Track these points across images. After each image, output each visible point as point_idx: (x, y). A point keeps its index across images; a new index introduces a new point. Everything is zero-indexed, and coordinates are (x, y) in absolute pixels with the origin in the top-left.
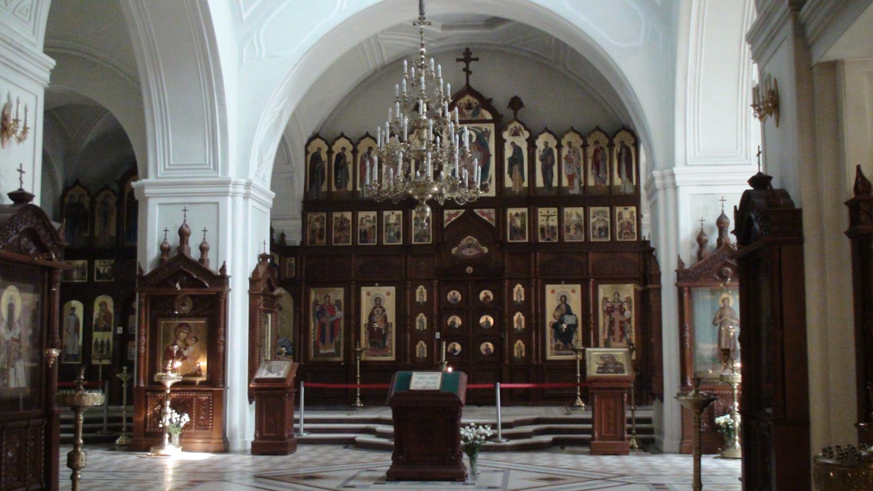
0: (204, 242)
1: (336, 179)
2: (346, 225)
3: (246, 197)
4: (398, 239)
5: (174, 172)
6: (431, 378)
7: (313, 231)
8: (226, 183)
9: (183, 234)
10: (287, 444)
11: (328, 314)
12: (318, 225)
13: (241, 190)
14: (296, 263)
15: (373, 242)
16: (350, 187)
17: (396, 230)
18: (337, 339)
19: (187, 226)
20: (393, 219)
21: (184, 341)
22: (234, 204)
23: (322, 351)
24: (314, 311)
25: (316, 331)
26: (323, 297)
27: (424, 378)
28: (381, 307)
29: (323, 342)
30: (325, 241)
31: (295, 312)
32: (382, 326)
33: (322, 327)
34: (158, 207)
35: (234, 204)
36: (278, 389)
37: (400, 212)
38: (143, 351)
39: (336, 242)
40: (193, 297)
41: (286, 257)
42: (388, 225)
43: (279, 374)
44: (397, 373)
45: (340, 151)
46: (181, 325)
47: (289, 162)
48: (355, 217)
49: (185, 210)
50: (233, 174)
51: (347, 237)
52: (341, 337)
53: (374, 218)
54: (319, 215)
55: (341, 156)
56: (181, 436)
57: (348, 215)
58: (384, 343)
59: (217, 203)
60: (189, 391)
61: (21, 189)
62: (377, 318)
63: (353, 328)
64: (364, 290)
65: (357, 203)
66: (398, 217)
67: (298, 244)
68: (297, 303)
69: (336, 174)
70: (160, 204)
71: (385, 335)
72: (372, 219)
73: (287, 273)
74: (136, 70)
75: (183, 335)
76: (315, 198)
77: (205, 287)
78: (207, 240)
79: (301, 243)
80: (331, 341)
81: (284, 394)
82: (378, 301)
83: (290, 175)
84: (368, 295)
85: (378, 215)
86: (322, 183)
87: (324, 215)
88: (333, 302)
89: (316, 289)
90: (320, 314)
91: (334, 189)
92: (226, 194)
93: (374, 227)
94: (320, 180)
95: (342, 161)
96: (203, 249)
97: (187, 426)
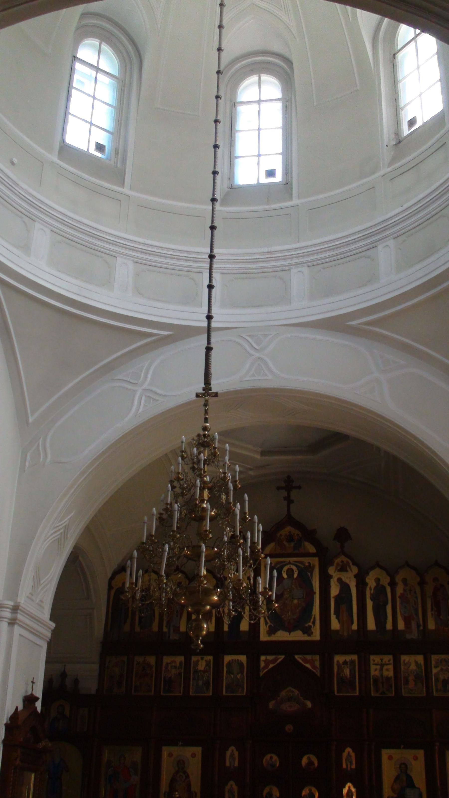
3: (12, 623)
16: (155, 627)
20: (202, 666)
28: (185, 772)
37: (211, 658)
42: (196, 671)
48: (159, 662)
53: (181, 663)
57: (152, 660)
61: (32, 694)
64: (166, 750)
66: (208, 663)
67: (93, 692)
72: (178, 665)
82: (181, 765)
84: (169, 755)
91: (137, 629)
93: (180, 674)
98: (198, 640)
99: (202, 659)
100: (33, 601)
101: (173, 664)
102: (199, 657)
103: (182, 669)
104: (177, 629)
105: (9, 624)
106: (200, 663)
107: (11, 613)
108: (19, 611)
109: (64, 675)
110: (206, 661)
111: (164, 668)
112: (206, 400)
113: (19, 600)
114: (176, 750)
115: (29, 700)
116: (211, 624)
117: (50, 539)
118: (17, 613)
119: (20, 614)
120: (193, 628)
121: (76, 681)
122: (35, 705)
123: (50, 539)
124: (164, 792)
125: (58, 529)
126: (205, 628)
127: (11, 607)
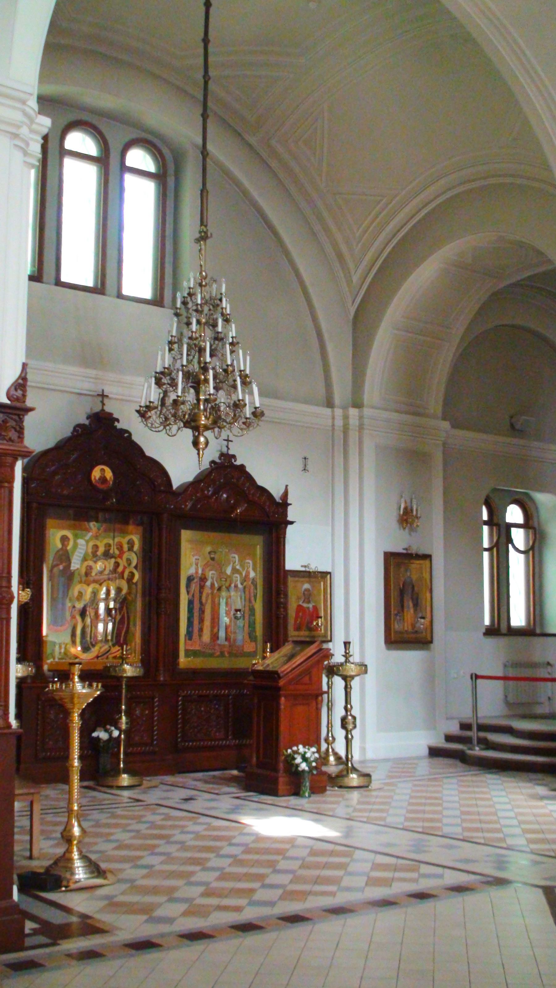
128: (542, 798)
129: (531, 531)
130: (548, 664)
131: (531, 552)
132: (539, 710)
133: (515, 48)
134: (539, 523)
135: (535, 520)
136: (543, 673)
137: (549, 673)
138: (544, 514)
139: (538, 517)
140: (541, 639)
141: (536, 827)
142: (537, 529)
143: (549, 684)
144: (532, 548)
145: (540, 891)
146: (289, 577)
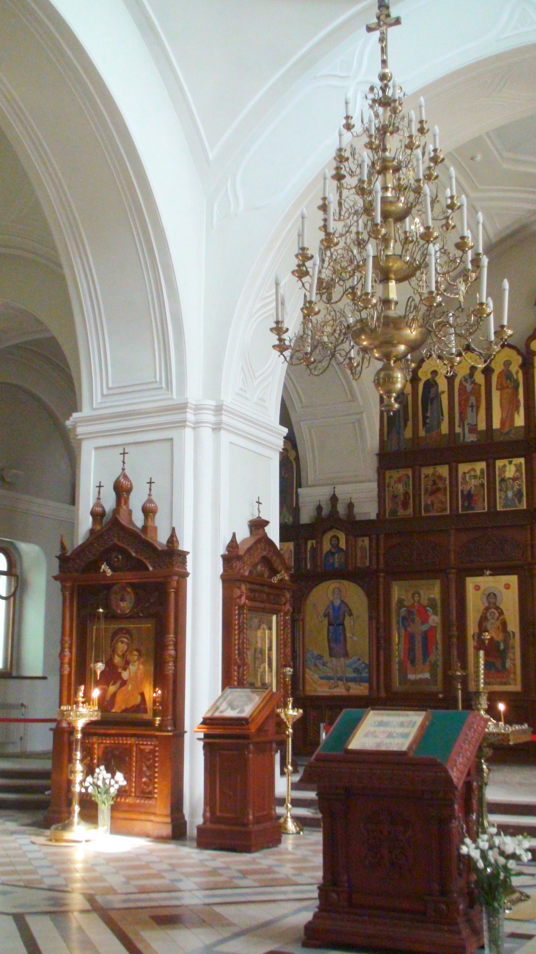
0: (150, 501)
1: (425, 418)
2: (440, 485)
3: (217, 428)
4: (520, 501)
5: (116, 398)
6: (402, 725)
7: (394, 497)
8: (182, 407)
9: (122, 490)
10: (249, 833)
11: (418, 620)
12: (400, 488)
13: (209, 417)
14: (370, 546)
15: (482, 507)
16: (445, 428)
17: (516, 487)
18: (432, 658)
19: (125, 477)
20: (510, 472)
21: (123, 656)
22: (197, 440)
23: (411, 677)
24: (398, 615)
25: (402, 646)
26: (410, 594)
27: (386, 724)
28: (497, 608)
29: (413, 662)
30: (410, 511)
31: (370, 618)
32: (499, 637)
33: (410, 638)
34: (93, 452)
35: (197, 440)
36: (238, 737)
37: (522, 460)
38: (66, 672)
39: (426, 511)
40: (133, 586)
41: (356, 536)
42: (503, 480)
43: (242, 711)
44: (344, 711)
45: (429, 376)
46: (121, 630)
47: (354, 398)
48: (454, 473)
49: (124, 453)
50: (195, 391)
51: (443, 503)
52: (437, 655)
53: (482, 471)
54: (402, 472)
55: (431, 385)
56: (114, 808)
57: (443, 471)
58: (504, 663)
59: (171, 440)
60: (126, 736)
61: (259, 517)
62: (492, 624)
63: (455, 640)
64: (471, 582)
65: (454, 452)
66: (518, 468)
67: (373, 517)
68: (373, 607)
69: (425, 410)
70: (96, 448)
71: (504, 650)
72: (478, 473)
73: (358, 561)
74: (54, 248)
75: (121, 647)
76: (395, 448)
77: (147, 569)
78: (154, 498)
79: (378, 515)
80: (424, 662)
81: (247, 746)
82: (492, 597)
83: (358, 416)
84: (478, 588)
85: (488, 466)
86: (406, 425)
87: (410, 472)
88: (425, 602)
89: (402, 583)
90: (406, 620)
91: (422, 433)
92: (182, 424)
93: (482, 485)
94: (402, 424)
95: (433, 391)
96: (148, 511)
97: (122, 792)
98: (389, 397)
99: (510, 463)
100: (247, 399)
101: (472, 473)
102: (505, 462)
103: (483, 478)
104: (473, 429)
105: (213, 429)
106: (507, 469)
107: (215, 415)
108: (223, 412)
109: (334, 499)
110: (515, 465)
111: (460, 480)
112: (382, 33)
113: (222, 398)
114: (487, 582)
115: (258, 525)
116: (519, 415)
117: (258, 314)
118: (221, 414)
119: (225, 415)
120: (381, 381)
121: (350, 506)
122: (264, 530)
123: (258, 314)
124: (472, 633)
125: (266, 301)
126: (399, 380)
127: (213, 408)
128: (12, 833)
129: (13, 579)
130: (22, 705)
131: (12, 598)
132: (10, 749)
133: (43, 154)
134: (22, 572)
135: (18, 567)
136: (15, 714)
137: (23, 715)
138: (27, 563)
139: (21, 565)
140: (17, 681)
141: (7, 860)
142: (19, 576)
143: (22, 724)
144: (14, 594)
145: (11, 918)
146: (423, 713)
